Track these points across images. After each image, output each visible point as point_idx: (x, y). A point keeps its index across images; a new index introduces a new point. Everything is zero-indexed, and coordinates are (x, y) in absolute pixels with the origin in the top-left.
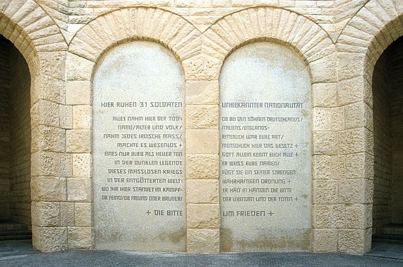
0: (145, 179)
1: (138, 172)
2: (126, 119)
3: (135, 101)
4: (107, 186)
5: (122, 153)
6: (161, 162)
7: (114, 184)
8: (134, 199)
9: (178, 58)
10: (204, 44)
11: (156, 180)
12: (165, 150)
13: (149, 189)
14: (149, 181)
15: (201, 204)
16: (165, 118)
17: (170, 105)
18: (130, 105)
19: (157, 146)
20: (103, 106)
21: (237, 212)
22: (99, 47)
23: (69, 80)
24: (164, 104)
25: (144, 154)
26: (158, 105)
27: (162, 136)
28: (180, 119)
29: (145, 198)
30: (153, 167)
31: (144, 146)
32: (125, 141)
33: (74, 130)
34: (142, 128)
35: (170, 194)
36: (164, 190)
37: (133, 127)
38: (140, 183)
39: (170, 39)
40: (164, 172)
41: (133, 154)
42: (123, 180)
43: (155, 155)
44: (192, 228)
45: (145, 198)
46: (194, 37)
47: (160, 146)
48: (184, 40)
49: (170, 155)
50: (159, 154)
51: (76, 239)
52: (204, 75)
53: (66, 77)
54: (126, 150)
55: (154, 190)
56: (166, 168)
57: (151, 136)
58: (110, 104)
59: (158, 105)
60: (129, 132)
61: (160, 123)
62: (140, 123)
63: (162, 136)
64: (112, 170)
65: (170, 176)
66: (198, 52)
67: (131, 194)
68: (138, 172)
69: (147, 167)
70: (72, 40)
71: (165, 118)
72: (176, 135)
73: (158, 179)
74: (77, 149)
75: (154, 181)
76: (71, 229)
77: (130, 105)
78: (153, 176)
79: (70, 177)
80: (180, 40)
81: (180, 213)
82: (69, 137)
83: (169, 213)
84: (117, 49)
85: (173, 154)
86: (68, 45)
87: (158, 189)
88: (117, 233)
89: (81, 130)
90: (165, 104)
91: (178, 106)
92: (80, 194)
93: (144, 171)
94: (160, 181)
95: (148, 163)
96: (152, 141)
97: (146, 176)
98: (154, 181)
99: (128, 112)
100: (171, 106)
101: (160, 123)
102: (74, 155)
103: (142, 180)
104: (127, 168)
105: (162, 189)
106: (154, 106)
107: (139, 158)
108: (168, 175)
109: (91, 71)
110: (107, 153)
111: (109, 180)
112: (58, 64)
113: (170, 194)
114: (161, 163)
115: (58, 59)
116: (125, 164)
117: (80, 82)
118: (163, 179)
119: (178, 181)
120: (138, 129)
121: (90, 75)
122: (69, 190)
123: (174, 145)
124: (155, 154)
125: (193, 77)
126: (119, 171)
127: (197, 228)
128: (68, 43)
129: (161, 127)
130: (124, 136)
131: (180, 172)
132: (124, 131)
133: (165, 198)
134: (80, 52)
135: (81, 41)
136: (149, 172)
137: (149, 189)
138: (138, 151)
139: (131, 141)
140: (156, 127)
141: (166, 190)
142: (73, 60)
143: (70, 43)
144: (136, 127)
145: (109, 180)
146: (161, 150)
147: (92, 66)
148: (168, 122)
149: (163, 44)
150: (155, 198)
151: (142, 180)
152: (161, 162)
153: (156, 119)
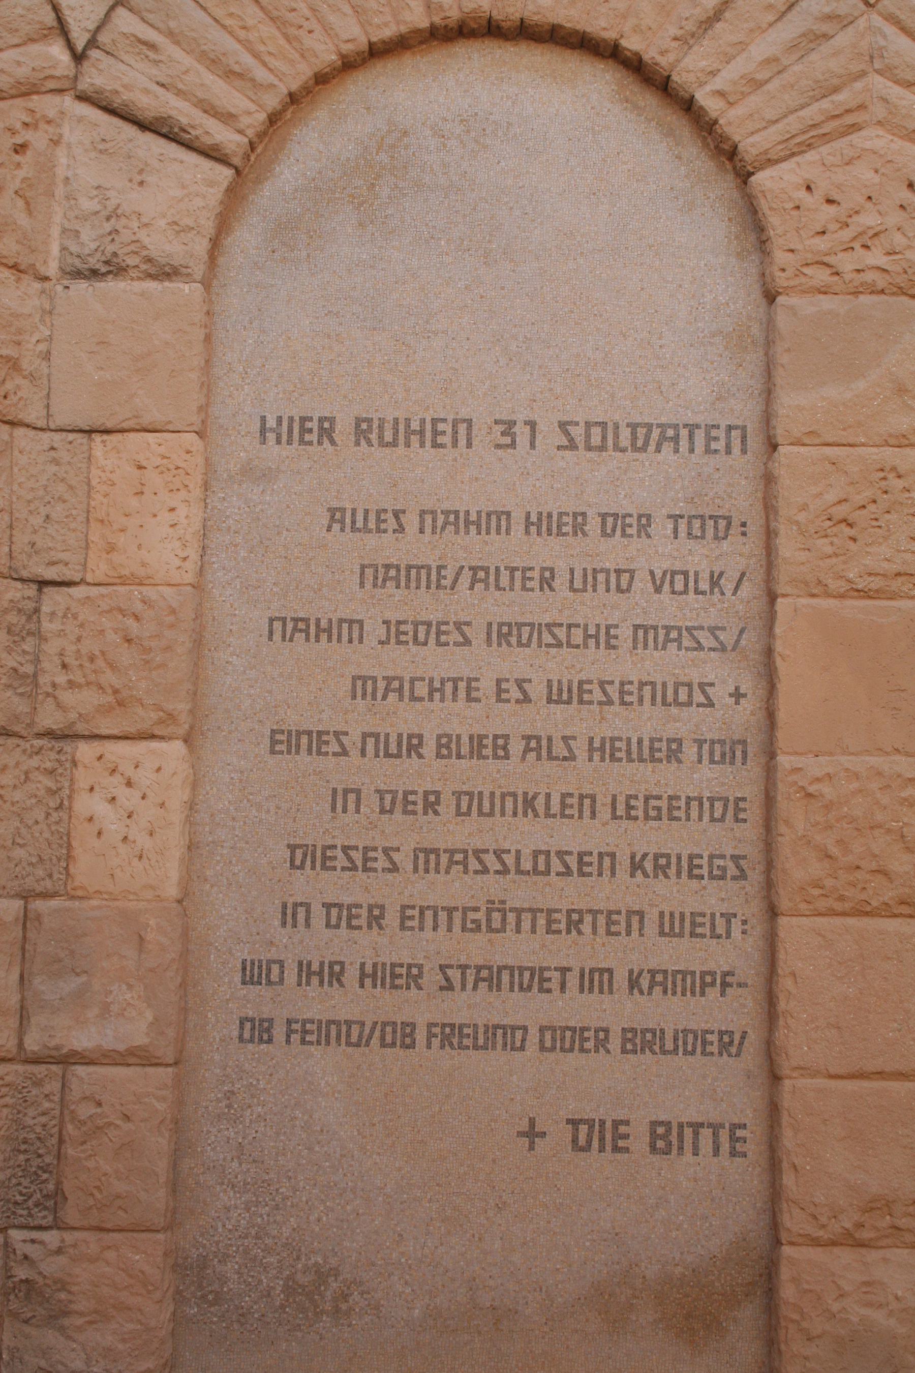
0: (519, 911)
1: (473, 864)
2: (411, 521)
3: (464, 413)
4: (273, 954)
5: (380, 746)
6: (621, 799)
7: (320, 943)
8: (446, 1041)
9: (727, 154)
10: (887, 72)
11: (588, 918)
12: (646, 722)
13: (535, 979)
14: (542, 921)
15: (866, 1084)
16: (645, 521)
17: (676, 439)
18: (430, 433)
19: (598, 695)
20: (271, 436)
21: (289, 1022)
22: (261, 74)
23: (77, 274)
24: (641, 432)
25: (516, 747)
26: (589, 438)
27: (625, 633)
28: (735, 530)
29: (506, 1036)
30: (570, 836)
31: (515, 694)
32: (401, 661)
33: (94, 591)
34: (505, 581)
35: (669, 1012)
36: (633, 983)
37: (449, 573)
38: (481, 938)
39: (686, 41)
40: (636, 866)
41: (446, 747)
42: (376, 918)
43: (581, 753)
44: (816, 1242)
45: (506, 1036)
46: (825, 28)
47: (615, 697)
48: (761, 49)
49: (674, 754)
50: (607, 750)
51: (57, 1316)
52: (882, 261)
53: (55, 249)
54: (405, 718)
55: (573, 980)
56: (650, 838)
57: (561, 633)
58: (314, 424)
59: (589, 438)
60: (426, 605)
61: (613, 553)
62: (497, 550)
63: (625, 633)
64: (308, 851)
65: (672, 894)
66: (849, 119)
67: (420, 1008)
68: (473, 864)
69: (526, 835)
70: (98, 29)
71: (645, 521)
72: (713, 630)
73: (594, 913)
74: (105, 710)
75: (574, 925)
76: (32, 1251)
77: (430, 433)
78: (566, 893)
79: (46, 895)
80: (742, 46)
81: (733, 1139)
82: (61, 633)
83: (664, 1138)
84: (473, 62)
85: (690, 751)
86: (78, 58)
87: (596, 979)
88: (322, 1275)
89: (136, 591)
90: (644, 438)
91: (720, 445)
92: (106, 1008)
93: (509, 860)
94: (609, 923)
95: (540, 803)
96: (558, 665)
97: (521, 893)
98: (574, 925)
99: (426, 478)
100: (684, 444)
101: (613, 553)
102: (85, 751)
103: (496, 917)
104: (405, 834)
105: (621, 979)
106: (580, 440)
107: (482, 776)
108: (661, 886)
109: (209, 226)
110: (284, 741)
111: (291, 914)
112: (21, 173)
113: (669, 1012)
114: (621, 811)
115: (20, 149)
116: (398, 815)
117: (138, 286)
118: (630, 913)
119: (720, 923)
120: (479, 586)
121: (201, 246)
122: (39, 983)
123: (699, 698)
124: (580, 748)
125: (821, 276)
126: (357, 856)
127: (851, 1240)
128: (80, 46)
129: (621, 580)
130: (396, 633)
131: (732, 870)
132: (400, 604)
133: (640, 1040)
134: (150, 102)
135: (151, 35)
136: (541, 864)
137: (535, 979)
138: (477, 730)
139: (434, 662)
140: (587, 580)
141: (645, 983)
142: (102, 149)
143: (92, 43)
144: (466, 575)
145: (291, 914)
146: (619, 723)
147: (215, 195)
148: (662, 550)
149: (636, 67)
150: (567, 1039)
151: (496, 917)
152: (621, 799)
153: (593, 525)
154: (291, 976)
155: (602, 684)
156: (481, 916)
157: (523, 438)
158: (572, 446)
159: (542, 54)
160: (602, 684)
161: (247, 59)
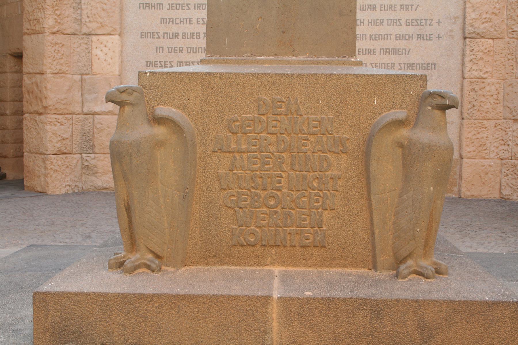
139: (181, 14)
160: (160, 62)
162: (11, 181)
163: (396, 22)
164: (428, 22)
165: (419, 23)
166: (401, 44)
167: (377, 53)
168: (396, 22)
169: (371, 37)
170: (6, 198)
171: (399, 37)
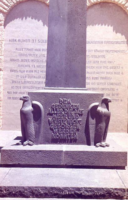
97: (33, 85)
130: (22, 61)
139: (26, 63)
154: (12, 93)
155: (32, 82)
156: (30, 87)
157: (35, 41)
158: (39, 42)
159: (98, 6)
160: (32, 82)
161: (8, 3)
162: (97, 111)
163: (106, 67)
164: (118, 67)
165: (115, 68)
166: (109, 76)
167: (99, 79)
168: (106, 67)
169: (97, 73)
170: (27, 130)
171: (107, 73)
